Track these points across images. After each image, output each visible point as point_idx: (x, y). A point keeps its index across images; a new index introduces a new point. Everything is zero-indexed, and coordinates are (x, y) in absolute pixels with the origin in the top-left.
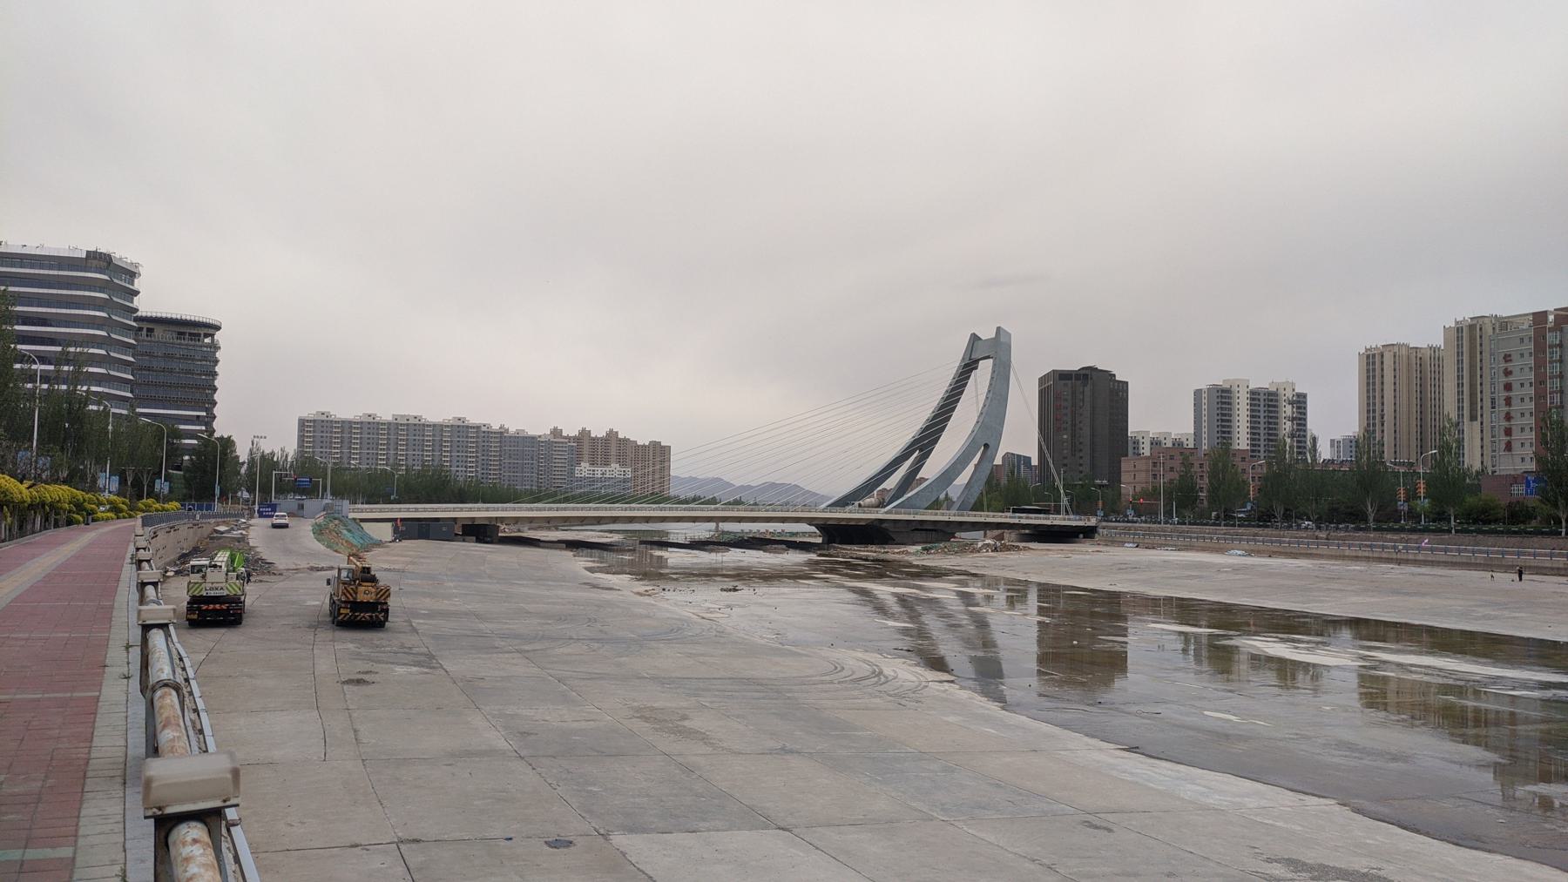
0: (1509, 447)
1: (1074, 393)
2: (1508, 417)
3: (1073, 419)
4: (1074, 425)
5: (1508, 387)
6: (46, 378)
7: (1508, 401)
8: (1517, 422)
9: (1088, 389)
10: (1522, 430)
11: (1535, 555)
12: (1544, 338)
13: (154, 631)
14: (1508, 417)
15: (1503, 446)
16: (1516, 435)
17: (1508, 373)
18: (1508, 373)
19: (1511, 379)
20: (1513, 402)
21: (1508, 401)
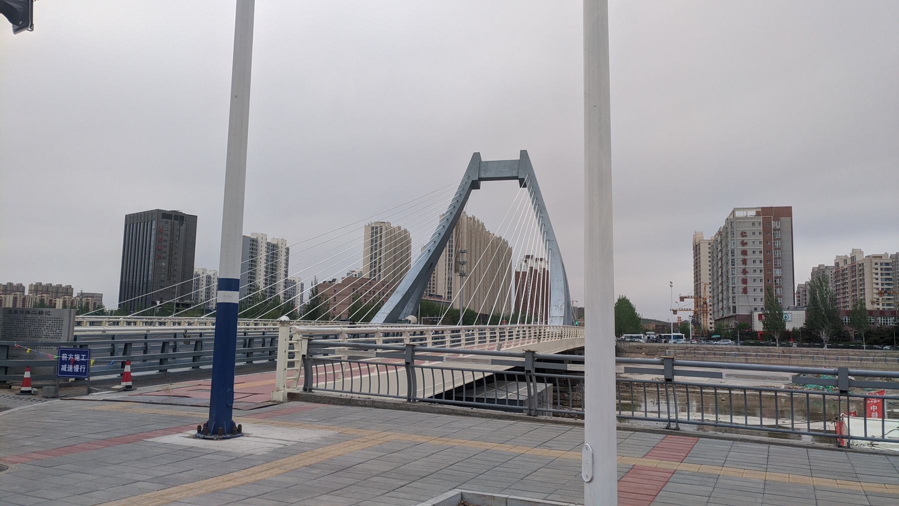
0: (745, 291)
1: (172, 230)
2: (745, 272)
3: (171, 250)
4: (171, 255)
5: (744, 253)
6: (75, 363)
7: (744, 262)
8: (750, 275)
9: (183, 227)
10: (754, 280)
11: (873, 360)
12: (770, 224)
13: (470, 210)
14: (745, 272)
15: (741, 290)
16: (750, 284)
17: (744, 244)
18: (744, 244)
19: (746, 248)
20: (748, 262)
21: (744, 262)
